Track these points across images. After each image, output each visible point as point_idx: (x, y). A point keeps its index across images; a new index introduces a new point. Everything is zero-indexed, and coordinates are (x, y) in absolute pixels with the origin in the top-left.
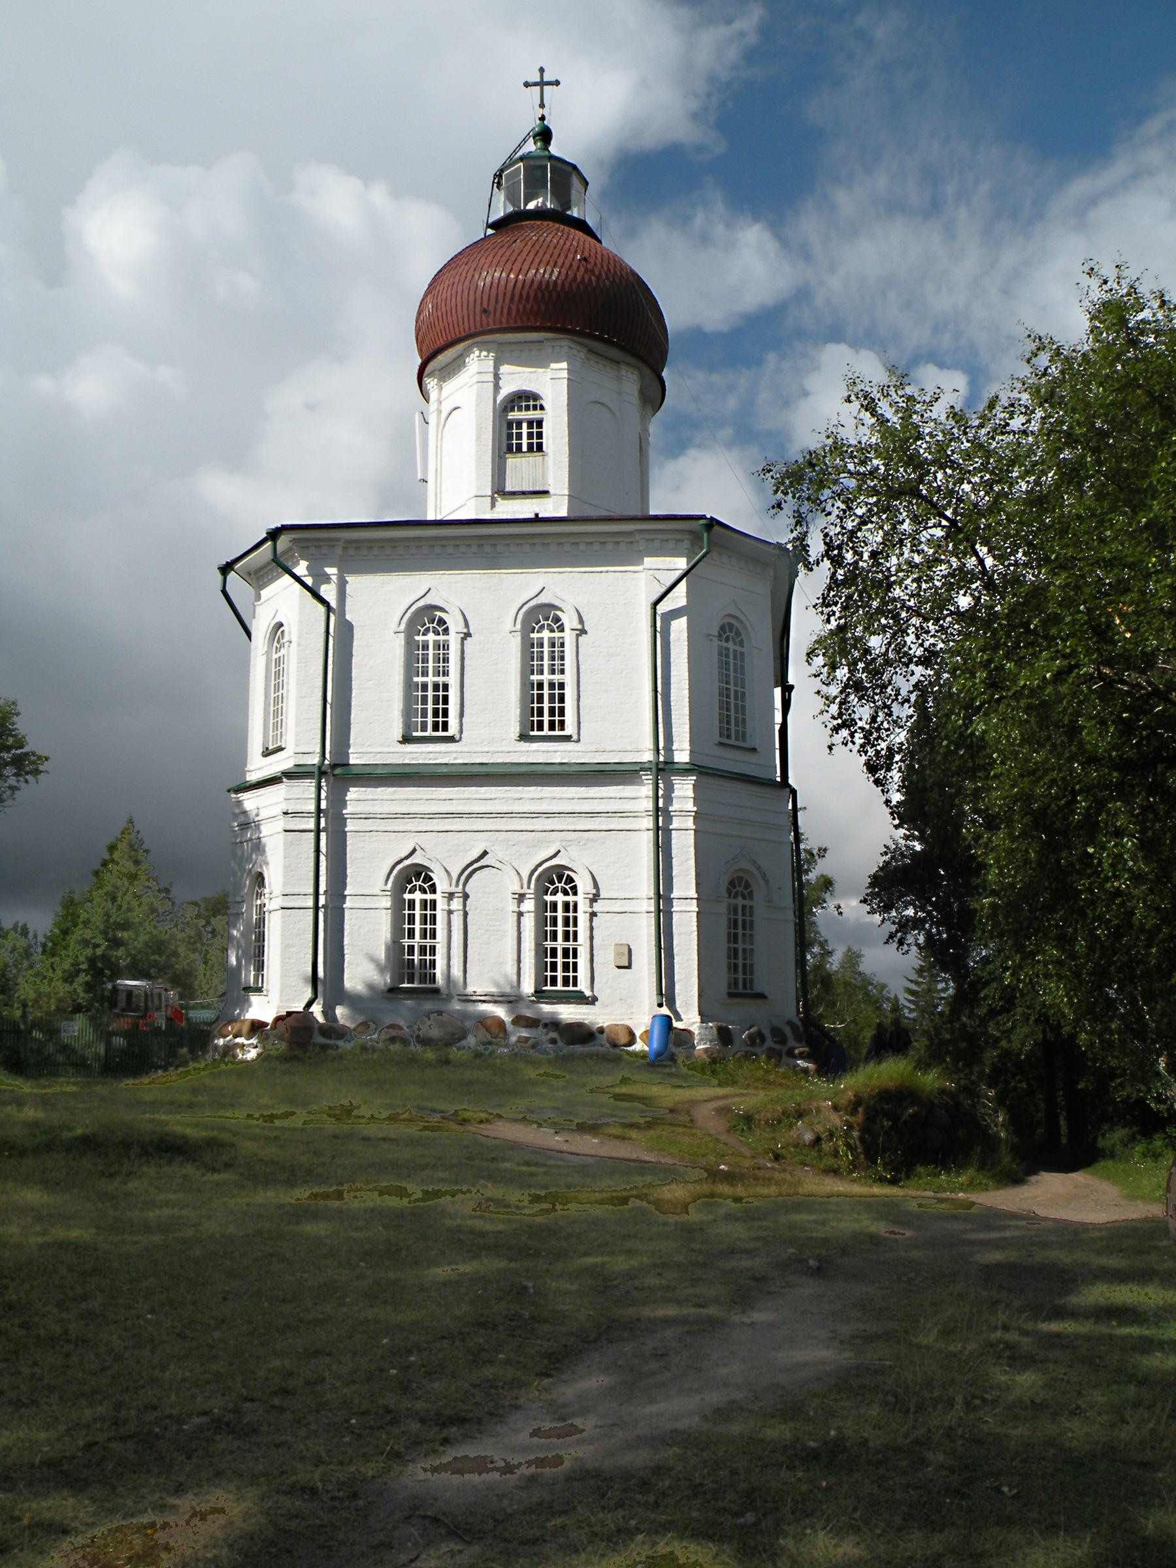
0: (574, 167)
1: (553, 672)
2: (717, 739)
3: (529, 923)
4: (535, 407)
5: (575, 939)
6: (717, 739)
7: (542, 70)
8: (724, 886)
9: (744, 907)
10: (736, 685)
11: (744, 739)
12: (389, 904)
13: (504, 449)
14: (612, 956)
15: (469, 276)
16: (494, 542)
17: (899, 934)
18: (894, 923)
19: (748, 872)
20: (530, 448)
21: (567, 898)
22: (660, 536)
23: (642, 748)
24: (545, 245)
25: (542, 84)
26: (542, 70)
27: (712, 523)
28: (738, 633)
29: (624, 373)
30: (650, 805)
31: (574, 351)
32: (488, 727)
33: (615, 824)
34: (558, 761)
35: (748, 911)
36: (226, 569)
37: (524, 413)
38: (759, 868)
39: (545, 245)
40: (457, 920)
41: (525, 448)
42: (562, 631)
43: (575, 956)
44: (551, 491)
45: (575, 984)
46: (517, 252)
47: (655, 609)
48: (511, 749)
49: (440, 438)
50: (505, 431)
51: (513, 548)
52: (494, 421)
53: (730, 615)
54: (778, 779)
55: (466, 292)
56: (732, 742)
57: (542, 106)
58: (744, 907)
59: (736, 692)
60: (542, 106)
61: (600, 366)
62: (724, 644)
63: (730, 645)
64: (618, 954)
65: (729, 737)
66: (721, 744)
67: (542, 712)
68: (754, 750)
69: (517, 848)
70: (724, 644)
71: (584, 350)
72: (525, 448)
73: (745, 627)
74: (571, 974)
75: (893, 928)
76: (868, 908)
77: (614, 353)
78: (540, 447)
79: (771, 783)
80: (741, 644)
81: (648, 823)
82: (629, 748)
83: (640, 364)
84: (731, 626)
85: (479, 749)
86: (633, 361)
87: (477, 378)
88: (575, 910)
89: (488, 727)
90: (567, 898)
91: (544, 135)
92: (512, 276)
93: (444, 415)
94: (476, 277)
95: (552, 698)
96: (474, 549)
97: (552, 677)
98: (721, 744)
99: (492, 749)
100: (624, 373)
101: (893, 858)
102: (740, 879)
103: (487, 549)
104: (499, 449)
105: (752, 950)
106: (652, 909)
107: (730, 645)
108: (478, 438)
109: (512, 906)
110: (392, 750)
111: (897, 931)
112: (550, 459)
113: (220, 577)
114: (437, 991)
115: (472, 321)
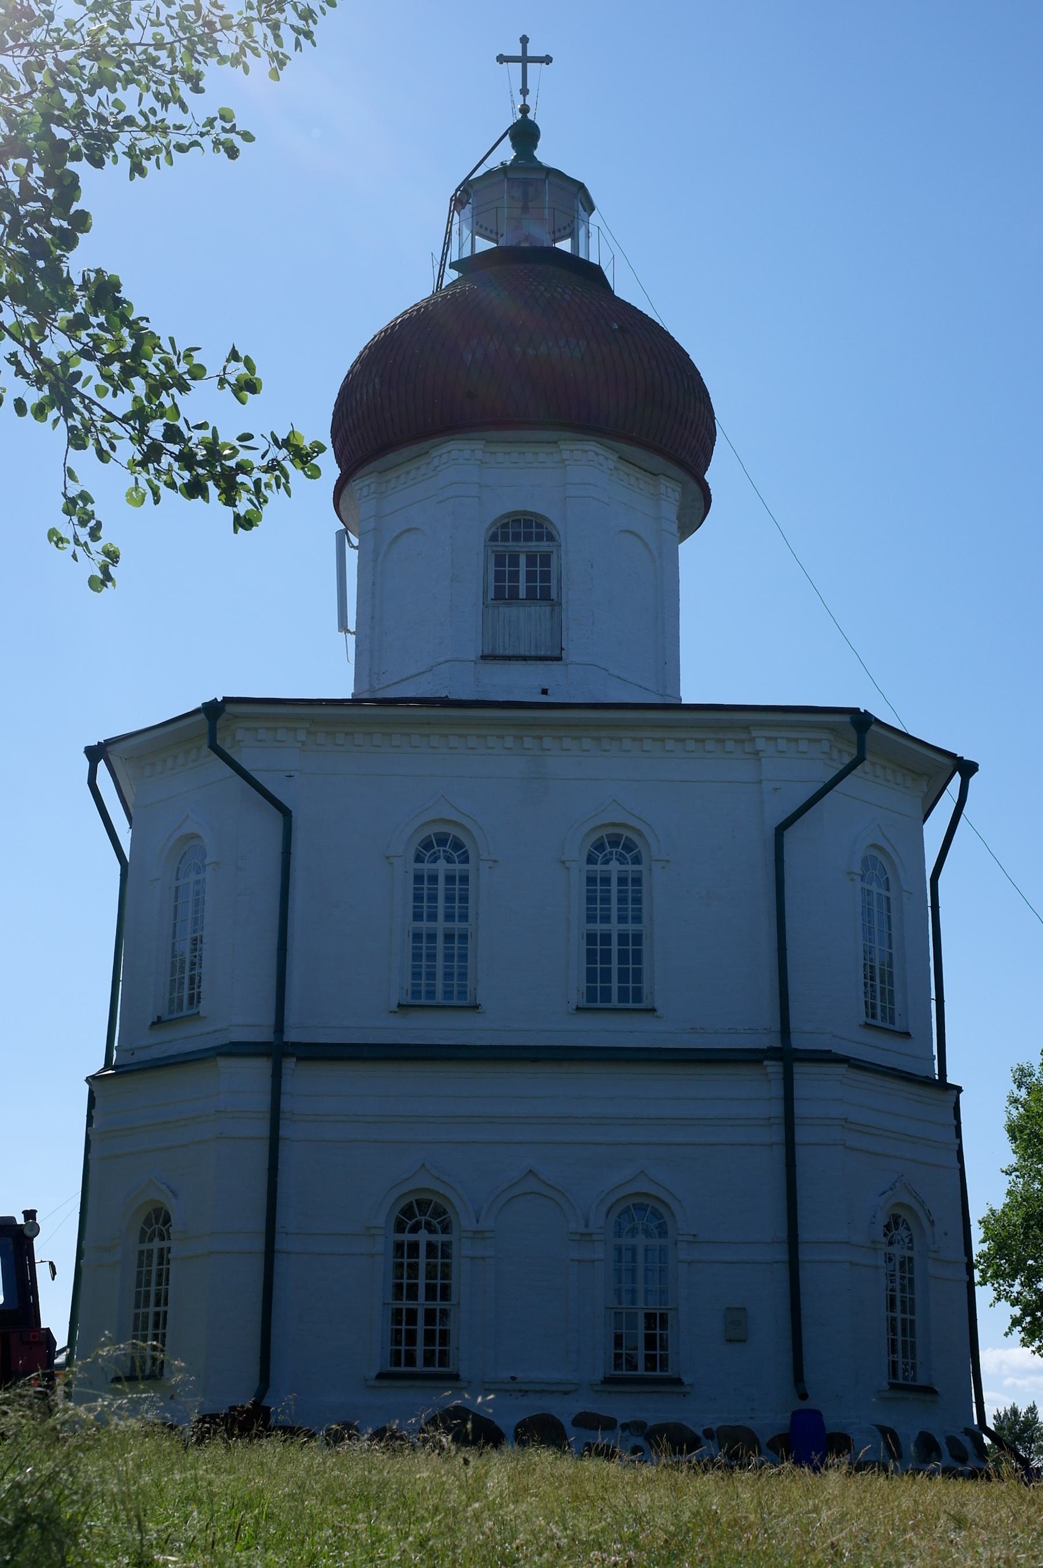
1: (622, 919)
2: (863, 1018)
6: (863, 1018)
7: (524, 40)
13: (491, 594)
20: (531, 595)
25: (524, 60)
26: (524, 40)
29: (566, 455)
36: (94, 754)
37: (522, 543)
38: (922, 1204)
41: (522, 594)
42: (466, 861)
53: (874, 846)
54: (937, 1077)
56: (878, 1022)
57: (524, 91)
60: (524, 91)
65: (874, 1016)
67: (614, 969)
71: (614, 457)
72: (522, 594)
77: (656, 462)
79: (927, 1082)
86: (675, 471)
91: (524, 134)
95: (623, 957)
96: (509, 742)
98: (867, 1025)
104: (485, 593)
113: (86, 764)
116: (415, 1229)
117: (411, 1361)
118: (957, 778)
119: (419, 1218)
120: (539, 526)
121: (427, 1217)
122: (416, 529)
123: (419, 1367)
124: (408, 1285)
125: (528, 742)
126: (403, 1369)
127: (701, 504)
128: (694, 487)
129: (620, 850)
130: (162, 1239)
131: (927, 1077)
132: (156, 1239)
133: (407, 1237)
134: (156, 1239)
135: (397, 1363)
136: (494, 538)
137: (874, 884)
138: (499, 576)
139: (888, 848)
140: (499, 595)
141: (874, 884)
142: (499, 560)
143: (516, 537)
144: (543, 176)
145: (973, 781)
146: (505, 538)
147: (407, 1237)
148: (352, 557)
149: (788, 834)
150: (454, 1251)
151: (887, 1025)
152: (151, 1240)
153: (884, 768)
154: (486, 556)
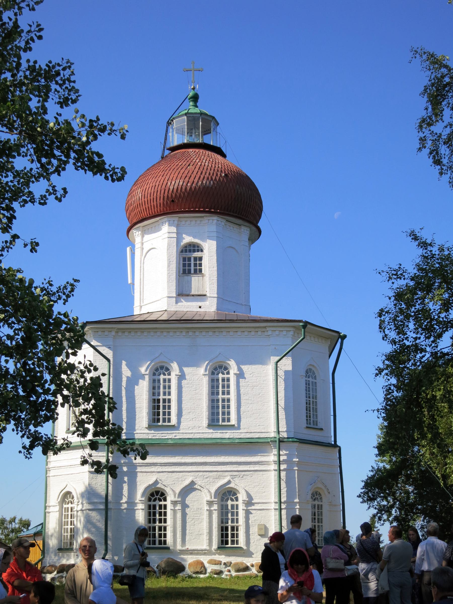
0: (213, 118)
1: (223, 393)
3: (215, 516)
4: (198, 251)
5: (237, 522)
8: (310, 496)
9: (318, 505)
10: (313, 398)
11: (317, 425)
12: (143, 507)
13: (181, 272)
14: (257, 530)
15: (165, 183)
16: (194, 331)
17: (379, 515)
18: (375, 508)
19: (321, 488)
21: (233, 503)
22: (279, 329)
23: (270, 431)
24: (205, 168)
27: (306, 324)
28: (314, 373)
30: (276, 459)
31: (219, 222)
32: (193, 422)
33: (257, 467)
34: (228, 437)
35: (320, 507)
39: (205, 168)
40: (179, 515)
41: (192, 271)
43: (237, 530)
44: (208, 295)
45: (237, 544)
46: (191, 172)
47: (277, 365)
48: (204, 431)
49: (142, 263)
50: (182, 262)
51: (204, 333)
52: (177, 258)
53: (310, 365)
55: (157, 187)
58: (318, 505)
59: (313, 401)
61: (231, 228)
62: (308, 379)
63: (310, 379)
64: (260, 529)
65: (310, 424)
66: (307, 427)
68: (322, 429)
69: (208, 479)
70: (308, 379)
71: (224, 221)
72: (192, 271)
73: (315, 367)
74: (235, 539)
75: (375, 511)
76: (361, 500)
77: (240, 222)
78: (201, 271)
79: (328, 445)
80: (315, 378)
81: (274, 467)
82: (263, 431)
83: (251, 226)
84: (310, 369)
85: (187, 432)
87: (167, 235)
88: (237, 509)
89: (193, 422)
90: (233, 503)
92: (189, 185)
93: (145, 251)
94: (169, 184)
96: (184, 334)
97: (223, 396)
98: (307, 427)
99: (194, 431)
100: (242, 230)
101: (376, 473)
102: (316, 493)
103: (191, 334)
104: (179, 272)
105: (322, 526)
106: (277, 507)
107: (310, 379)
108: (169, 266)
109: (206, 507)
110: (142, 432)
111: (377, 513)
112: (207, 278)
114: (168, 548)
115: (155, 194)
116: (155, 500)
117: (154, 543)
118: (340, 340)
119: (156, 497)
120: (198, 247)
121: (158, 496)
122: (155, 248)
123: (157, 545)
124: (162, 509)
125: (191, 334)
126: (151, 546)
127: (258, 233)
128: (254, 228)
129: (222, 370)
130: (72, 503)
131: (329, 443)
132: (70, 504)
133: (152, 503)
134: (70, 504)
135: (150, 544)
136: (182, 251)
137: (311, 378)
138: (184, 265)
139: (316, 365)
140: (184, 272)
141: (311, 378)
142: (184, 259)
143: (190, 251)
144: (199, 115)
145: (345, 341)
146: (186, 251)
147: (152, 503)
148: (130, 281)
149: (278, 363)
150: (318, 385)
151: (315, 427)
152: (68, 504)
153: (315, 337)
154: (180, 258)
